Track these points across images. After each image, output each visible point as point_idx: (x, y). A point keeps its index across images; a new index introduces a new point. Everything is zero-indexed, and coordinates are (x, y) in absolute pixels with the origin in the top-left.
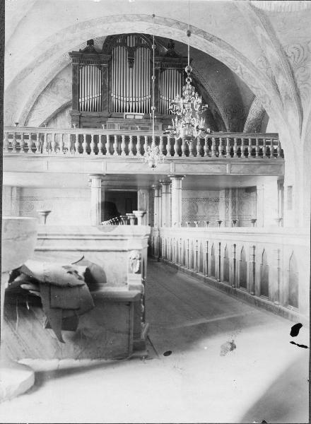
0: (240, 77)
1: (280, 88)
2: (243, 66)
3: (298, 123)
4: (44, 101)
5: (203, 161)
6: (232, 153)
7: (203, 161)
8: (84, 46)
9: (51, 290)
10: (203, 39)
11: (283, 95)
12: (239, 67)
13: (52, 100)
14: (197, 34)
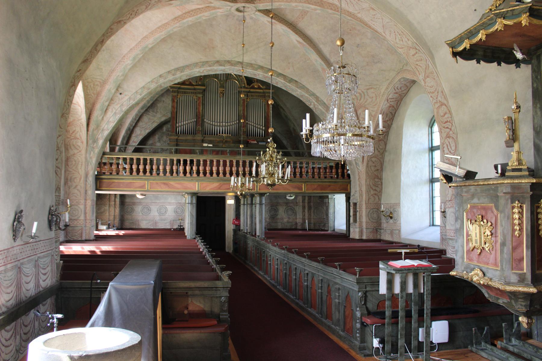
0: (314, 111)
2: (316, 103)
4: (145, 119)
9: (344, 227)
10: (283, 81)
12: (312, 104)
13: (151, 117)
14: (278, 77)
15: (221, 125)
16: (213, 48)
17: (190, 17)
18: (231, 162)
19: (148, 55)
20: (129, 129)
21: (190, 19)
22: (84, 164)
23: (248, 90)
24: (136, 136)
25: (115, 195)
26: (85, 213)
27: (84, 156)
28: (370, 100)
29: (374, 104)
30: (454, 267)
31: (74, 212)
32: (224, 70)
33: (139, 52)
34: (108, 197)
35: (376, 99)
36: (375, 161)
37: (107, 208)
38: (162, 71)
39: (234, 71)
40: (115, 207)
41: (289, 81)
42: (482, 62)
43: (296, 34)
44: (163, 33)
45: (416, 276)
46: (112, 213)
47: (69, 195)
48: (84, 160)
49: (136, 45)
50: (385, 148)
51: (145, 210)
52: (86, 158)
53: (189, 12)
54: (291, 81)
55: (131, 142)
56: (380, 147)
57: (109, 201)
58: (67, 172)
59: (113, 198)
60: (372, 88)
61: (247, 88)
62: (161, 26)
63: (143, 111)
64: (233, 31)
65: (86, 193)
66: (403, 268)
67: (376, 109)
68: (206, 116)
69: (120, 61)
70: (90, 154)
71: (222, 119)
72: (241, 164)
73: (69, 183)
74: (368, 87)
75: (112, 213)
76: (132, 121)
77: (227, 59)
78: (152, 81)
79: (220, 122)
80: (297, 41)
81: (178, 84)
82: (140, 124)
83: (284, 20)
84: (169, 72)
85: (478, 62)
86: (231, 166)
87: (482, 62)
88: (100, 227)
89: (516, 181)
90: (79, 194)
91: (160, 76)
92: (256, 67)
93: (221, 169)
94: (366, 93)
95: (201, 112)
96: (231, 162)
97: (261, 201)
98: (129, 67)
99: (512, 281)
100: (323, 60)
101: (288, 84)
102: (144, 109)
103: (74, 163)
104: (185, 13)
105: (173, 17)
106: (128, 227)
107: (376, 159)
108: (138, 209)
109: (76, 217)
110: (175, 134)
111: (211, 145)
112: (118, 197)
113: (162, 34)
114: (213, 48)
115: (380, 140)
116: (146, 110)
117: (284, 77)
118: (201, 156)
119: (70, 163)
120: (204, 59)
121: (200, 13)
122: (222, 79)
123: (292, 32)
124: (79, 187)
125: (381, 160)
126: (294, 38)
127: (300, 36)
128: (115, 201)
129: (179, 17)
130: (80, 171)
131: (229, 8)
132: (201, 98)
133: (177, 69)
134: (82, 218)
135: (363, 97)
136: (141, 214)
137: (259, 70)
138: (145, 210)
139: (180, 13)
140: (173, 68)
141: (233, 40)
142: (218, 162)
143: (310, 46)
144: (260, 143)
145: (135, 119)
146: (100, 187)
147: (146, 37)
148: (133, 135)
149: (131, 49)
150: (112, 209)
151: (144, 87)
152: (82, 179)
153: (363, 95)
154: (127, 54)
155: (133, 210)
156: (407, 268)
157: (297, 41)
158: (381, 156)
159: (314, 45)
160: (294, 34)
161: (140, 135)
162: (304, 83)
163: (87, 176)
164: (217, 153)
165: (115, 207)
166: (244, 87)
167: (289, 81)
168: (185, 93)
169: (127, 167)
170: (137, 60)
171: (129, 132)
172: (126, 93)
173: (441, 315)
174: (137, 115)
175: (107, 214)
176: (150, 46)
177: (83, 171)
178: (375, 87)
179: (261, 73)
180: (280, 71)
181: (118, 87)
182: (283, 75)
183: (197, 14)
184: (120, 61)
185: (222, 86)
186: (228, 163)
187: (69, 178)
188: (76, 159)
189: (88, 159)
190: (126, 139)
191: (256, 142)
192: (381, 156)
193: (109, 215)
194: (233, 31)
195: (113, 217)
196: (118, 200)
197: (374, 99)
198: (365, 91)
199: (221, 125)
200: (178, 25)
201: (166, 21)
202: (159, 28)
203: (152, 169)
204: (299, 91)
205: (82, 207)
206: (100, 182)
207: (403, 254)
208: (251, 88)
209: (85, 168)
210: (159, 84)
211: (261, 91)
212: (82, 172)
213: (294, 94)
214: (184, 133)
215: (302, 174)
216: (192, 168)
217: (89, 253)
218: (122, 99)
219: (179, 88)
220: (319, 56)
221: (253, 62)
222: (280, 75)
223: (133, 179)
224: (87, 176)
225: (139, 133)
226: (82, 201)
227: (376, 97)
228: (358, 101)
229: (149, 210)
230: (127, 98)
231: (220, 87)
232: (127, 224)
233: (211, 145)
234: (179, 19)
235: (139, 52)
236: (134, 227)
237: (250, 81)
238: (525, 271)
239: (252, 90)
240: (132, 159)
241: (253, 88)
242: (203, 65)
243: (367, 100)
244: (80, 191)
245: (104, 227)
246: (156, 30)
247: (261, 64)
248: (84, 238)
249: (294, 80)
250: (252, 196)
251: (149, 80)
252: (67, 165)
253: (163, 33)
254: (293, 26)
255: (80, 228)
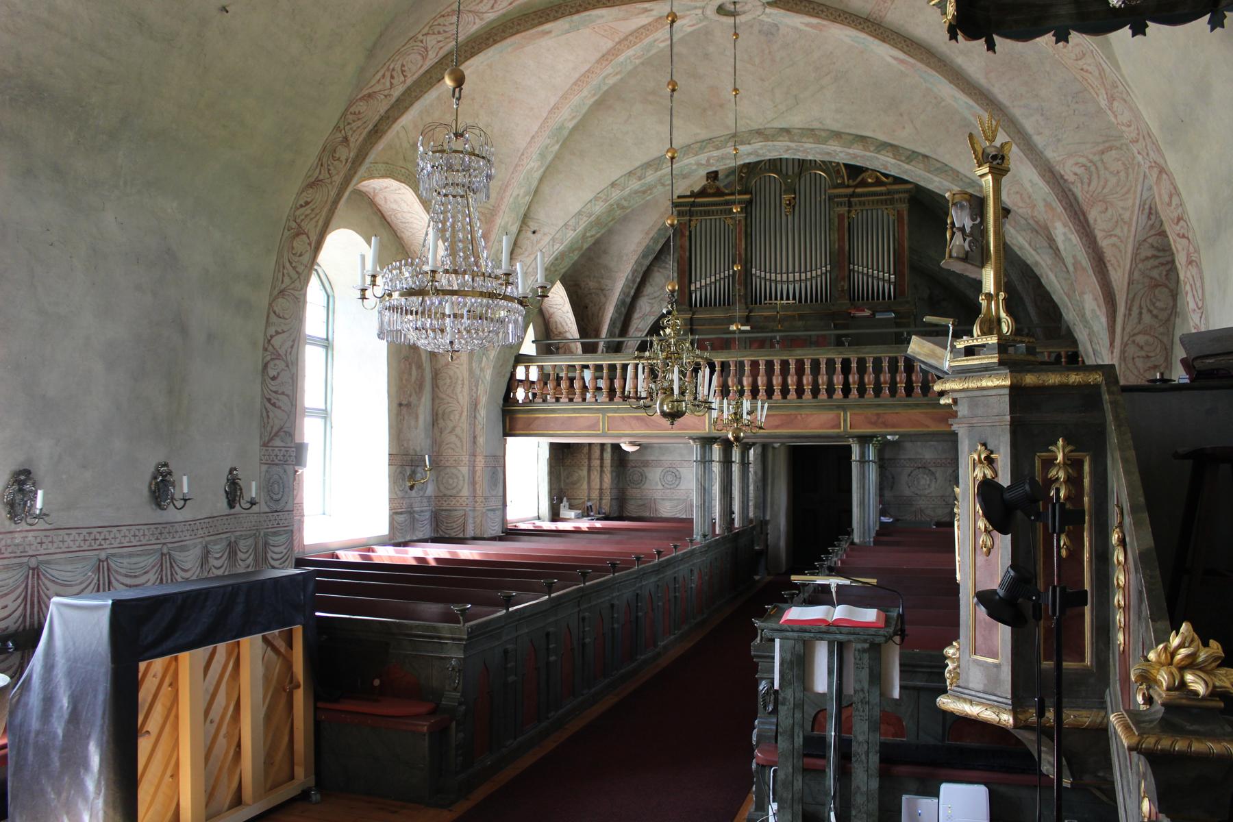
1: (1061, 247)
3: (1104, 320)
5: (908, 405)
6: (862, 391)
7: (908, 405)
8: (698, 181)
11: (1069, 261)
14: (878, 152)
15: (791, 278)
16: (721, 106)
17: (628, 48)
18: (785, 364)
19: (571, 143)
20: (622, 302)
21: (630, 52)
22: (466, 382)
23: (850, 190)
24: (643, 317)
25: (602, 445)
26: (474, 483)
27: (465, 366)
28: (1113, 180)
29: (1125, 189)
30: (957, 638)
31: (451, 481)
32: (755, 153)
33: (548, 141)
34: (586, 450)
35: (1127, 177)
36: (1147, 343)
37: (585, 473)
38: (615, 173)
39: (811, 151)
40: (602, 471)
41: (908, 158)
42: (1075, 37)
43: (884, 41)
44: (585, 93)
45: (839, 650)
46: (596, 484)
47: (440, 446)
48: (466, 375)
49: (540, 127)
50: (1175, 306)
51: (669, 478)
52: (471, 371)
53: (626, 39)
54: (912, 156)
55: (632, 331)
56: (1158, 304)
57: (590, 459)
58: (437, 401)
59: (596, 453)
60: (1111, 148)
61: (848, 186)
62: (579, 80)
63: (647, 262)
64: (757, 61)
65: (475, 443)
66: (807, 627)
67: (1130, 202)
68: (756, 261)
69: (517, 165)
70: (481, 362)
71: (792, 269)
72: (807, 366)
73: (441, 421)
74: (1101, 147)
75: (596, 484)
76: (626, 286)
77: (755, 126)
78: (596, 198)
79: (788, 273)
80: (896, 59)
81: (693, 195)
82: (649, 290)
83: (845, 12)
84: (630, 173)
85: (1062, 37)
86: (800, 371)
87: (1075, 37)
88: (565, 512)
89: (973, 384)
90: (459, 444)
91: (613, 185)
92: (823, 134)
93: (777, 380)
94: (1099, 164)
95: (743, 252)
96: (785, 364)
97: (862, 454)
98: (537, 175)
99: (971, 686)
100: (969, 95)
101: (907, 166)
102: (651, 258)
103: (448, 381)
104: (619, 42)
105: (599, 55)
106: (634, 515)
107: (1147, 337)
108: (655, 476)
109: (454, 491)
110: (687, 307)
111: (748, 328)
112: (609, 449)
113: (585, 97)
114: (721, 106)
115: (1157, 286)
116: (656, 259)
117: (894, 149)
118: (714, 354)
119: (441, 383)
120: (704, 134)
121: (647, 36)
122: (790, 173)
123: (870, 39)
124: (458, 431)
125: (1165, 340)
126: (884, 52)
127: (895, 46)
128: (602, 459)
129: (608, 52)
130: (460, 397)
131: (699, 12)
132: (743, 222)
133: (648, 165)
134: (465, 492)
135: (1095, 176)
136: (660, 487)
137: (831, 142)
138: (669, 478)
139: (610, 44)
140: (638, 164)
141: (762, 80)
142: (755, 365)
143: (928, 65)
144: (878, 316)
145: (634, 281)
146: (511, 429)
147: (556, 108)
148: (636, 315)
149: (533, 137)
150: (595, 475)
151: (580, 213)
152: (465, 414)
153: (1093, 168)
154: (526, 148)
155: (643, 476)
156: (796, 627)
157: (896, 59)
158: (1161, 329)
159: (940, 60)
160: (877, 42)
161: (650, 313)
162: (947, 159)
163: (475, 406)
164: (762, 344)
165: (602, 471)
166: (842, 185)
167: (908, 158)
168: (707, 213)
169: (602, 383)
170: (550, 158)
171: (624, 310)
172: (546, 230)
173: (967, 767)
174: (634, 271)
175: (585, 486)
176: (571, 125)
177: (467, 398)
178: (1117, 144)
179: (839, 149)
180: (882, 137)
181: (525, 219)
182: (891, 145)
183: (641, 40)
184: (517, 165)
185: (791, 189)
186: (777, 367)
187: (440, 412)
188: (451, 373)
189: (478, 372)
190: (619, 325)
191: (867, 313)
192: (1161, 329)
193: (589, 488)
194: (757, 61)
195: (597, 492)
196: (608, 456)
197: (1123, 174)
198: (1096, 158)
199: (791, 278)
200: (609, 70)
201: (587, 67)
202: (575, 84)
203: (800, 385)
204: (936, 179)
205: (465, 470)
206: (512, 420)
207: (833, 590)
208: (856, 186)
209: (471, 389)
210: (611, 201)
211: (883, 189)
212: (464, 398)
213: (930, 187)
214: (706, 304)
215: (913, 388)
216: (740, 382)
217: (414, 563)
218: (538, 242)
219: (693, 204)
220: (957, 85)
221: (816, 125)
222: (883, 146)
223: (574, 411)
224: (475, 406)
225: (648, 309)
226: (465, 459)
227: (1127, 169)
228: (1085, 186)
229: (678, 477)
230: (547, 239)
231: (786, 192)
232: (632, 509)
233: (748, 328)
234: (610, 58)
235: (548, 141)
236: (647, 514)
237: (854, 171)
238: (1088, 661)
239: (859, 190)
240: (612, 368)
241: (864, 184)
242: (702, 149)
243: (1106, 181)
244: (460, 438)
245: (572, 514)
246: (571, 88)
247: (836, 127)
248: (470, 533)
249: (919, 154)
250: (727, 445)
251: (591, 196)
252: (435, 385)
253: (585, 93)
254: (873, 24)
255: (462, 513)
